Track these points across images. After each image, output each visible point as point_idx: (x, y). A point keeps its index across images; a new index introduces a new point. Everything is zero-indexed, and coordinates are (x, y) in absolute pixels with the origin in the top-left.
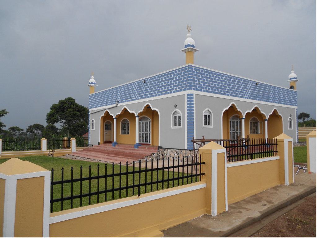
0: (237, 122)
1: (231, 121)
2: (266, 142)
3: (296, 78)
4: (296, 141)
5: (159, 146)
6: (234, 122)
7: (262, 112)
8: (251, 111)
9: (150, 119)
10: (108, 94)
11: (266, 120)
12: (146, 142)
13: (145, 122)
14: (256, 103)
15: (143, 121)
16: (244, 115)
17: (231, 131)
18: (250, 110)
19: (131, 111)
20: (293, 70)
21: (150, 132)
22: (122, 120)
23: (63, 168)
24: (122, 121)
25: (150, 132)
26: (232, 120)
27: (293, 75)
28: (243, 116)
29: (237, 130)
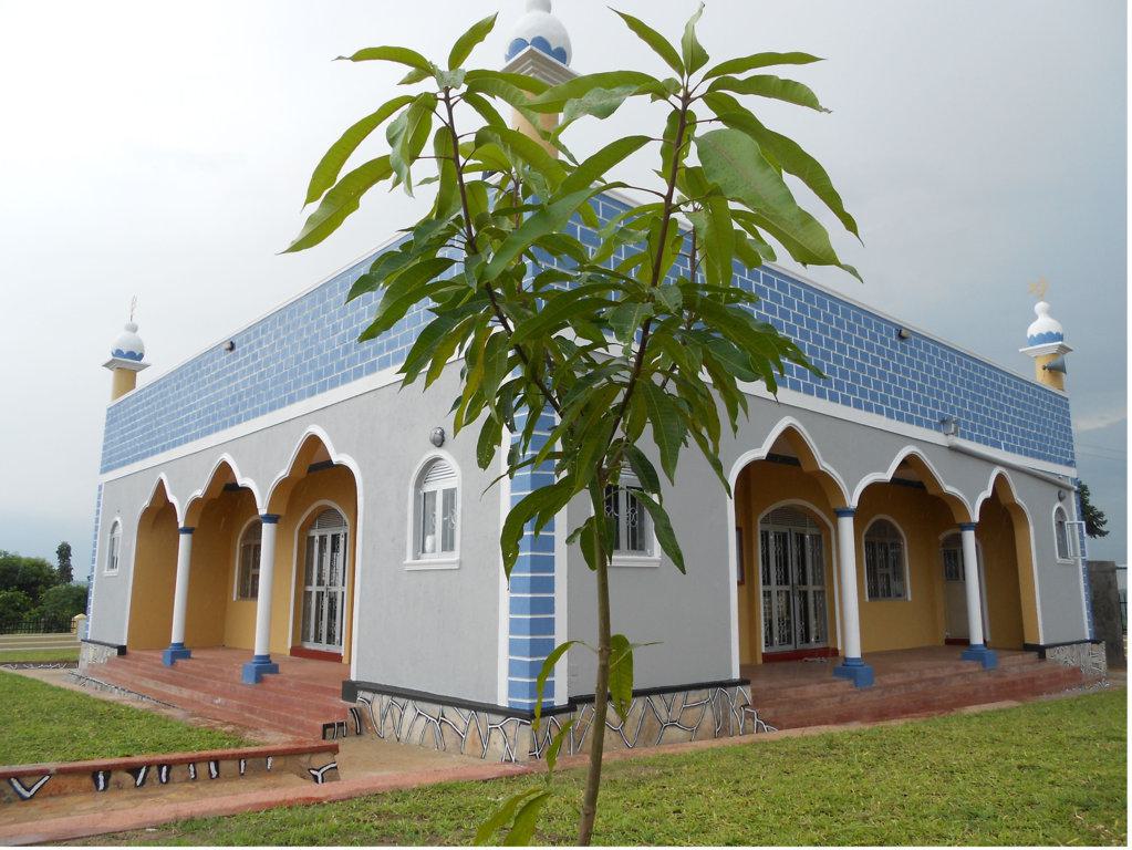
0: (801, 538)
1: (765, 536)
2: (224, 520)
3: (1059, 337)
4: (1084, 635)
5: (353, 678)
6: (782, 539)
7: (949, 489)
8: (888, 476)
9: (347, 521)
10: (155, 403)
11: (969, 526)
12: (328, 643)
13: (329, 533)
14: (921, 438)
15: (323, 532)
16: (851, 495)
17: (767, 581)
18: (885, 472)
19: (243, 476)
20: (1041, 298)
21: (767, 588)
22: (246, 526)
23: (684, 572)
24: (240, 536)
25: (767, 588)
26: (772, 530)
27: (1042, 324)
28: (847, 497)
29: (320, 595)
